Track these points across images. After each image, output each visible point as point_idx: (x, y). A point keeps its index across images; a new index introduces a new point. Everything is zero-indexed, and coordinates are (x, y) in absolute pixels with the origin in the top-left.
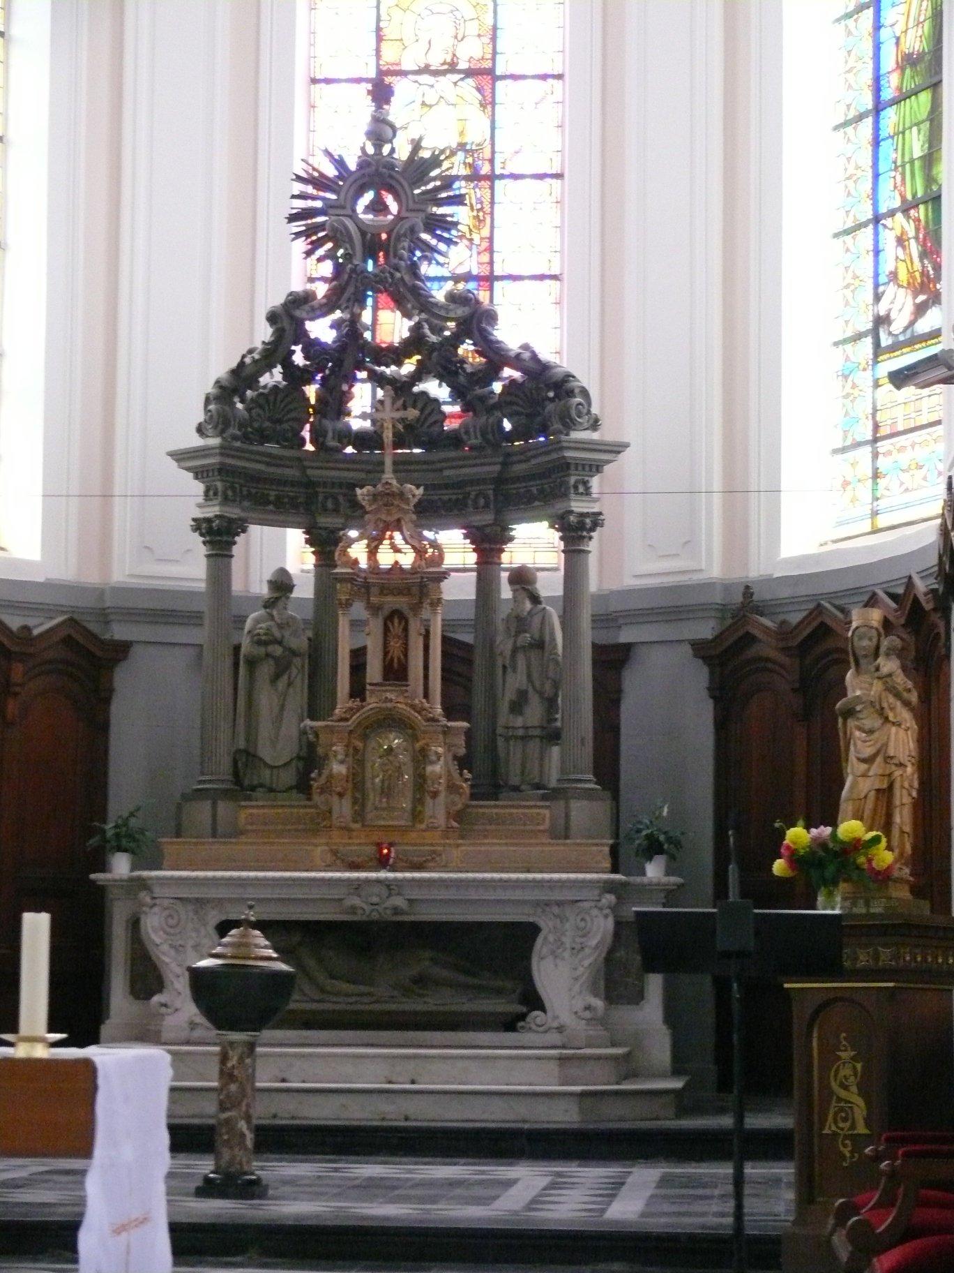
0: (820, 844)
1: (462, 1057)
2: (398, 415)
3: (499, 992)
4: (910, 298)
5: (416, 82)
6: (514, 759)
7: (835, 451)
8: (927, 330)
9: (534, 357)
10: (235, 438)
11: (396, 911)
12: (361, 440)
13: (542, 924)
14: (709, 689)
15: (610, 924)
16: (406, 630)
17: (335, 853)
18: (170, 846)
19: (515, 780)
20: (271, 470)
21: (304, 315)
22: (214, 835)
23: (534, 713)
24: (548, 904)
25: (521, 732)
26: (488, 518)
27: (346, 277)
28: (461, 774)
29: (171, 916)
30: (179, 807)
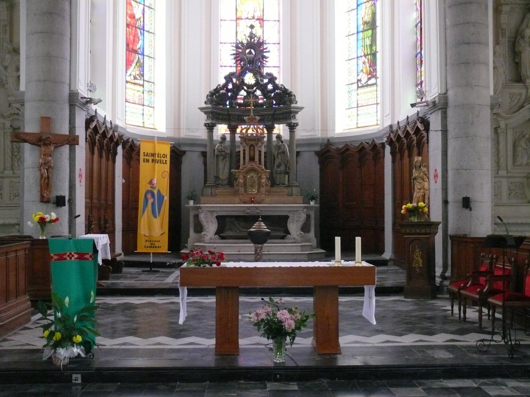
1: (279, 246)
2: (254, 100)
3: (279, 231)
4: (366, 76)
6: (278, 178)
7: (346, 109)
8: (371, 83)
9: (284, 88)
10: (214, 105)
11: (258, 213)
12: (240, 105)
13: (289, 215)
14: (319, 162)
15: (305, 216)
16: (254, 149)
17: (240, 200)
18: (202, 199)
19: (278, 183)
20: (222, 112)
22: (212, 196)
23: (282, 168)
24: (291, 211)
26: (270, 123)
27: (244, 69)
30: (202, 190)
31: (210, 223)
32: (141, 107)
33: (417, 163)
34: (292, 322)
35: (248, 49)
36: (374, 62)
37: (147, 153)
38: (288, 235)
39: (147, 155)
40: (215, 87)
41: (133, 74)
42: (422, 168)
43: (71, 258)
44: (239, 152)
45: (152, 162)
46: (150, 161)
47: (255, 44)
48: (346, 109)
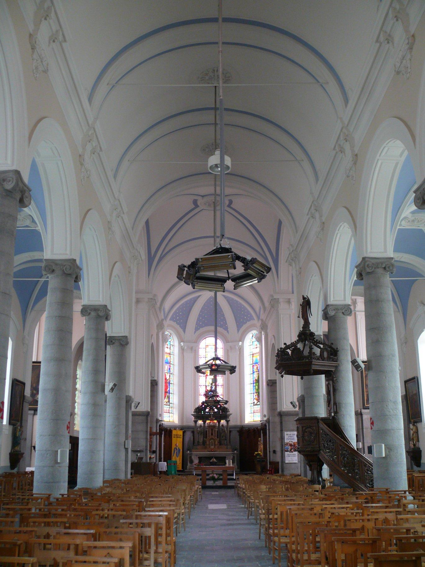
12: (207, 412)
32: (169, 414)
40: (197, 406)
44: (207, 431)
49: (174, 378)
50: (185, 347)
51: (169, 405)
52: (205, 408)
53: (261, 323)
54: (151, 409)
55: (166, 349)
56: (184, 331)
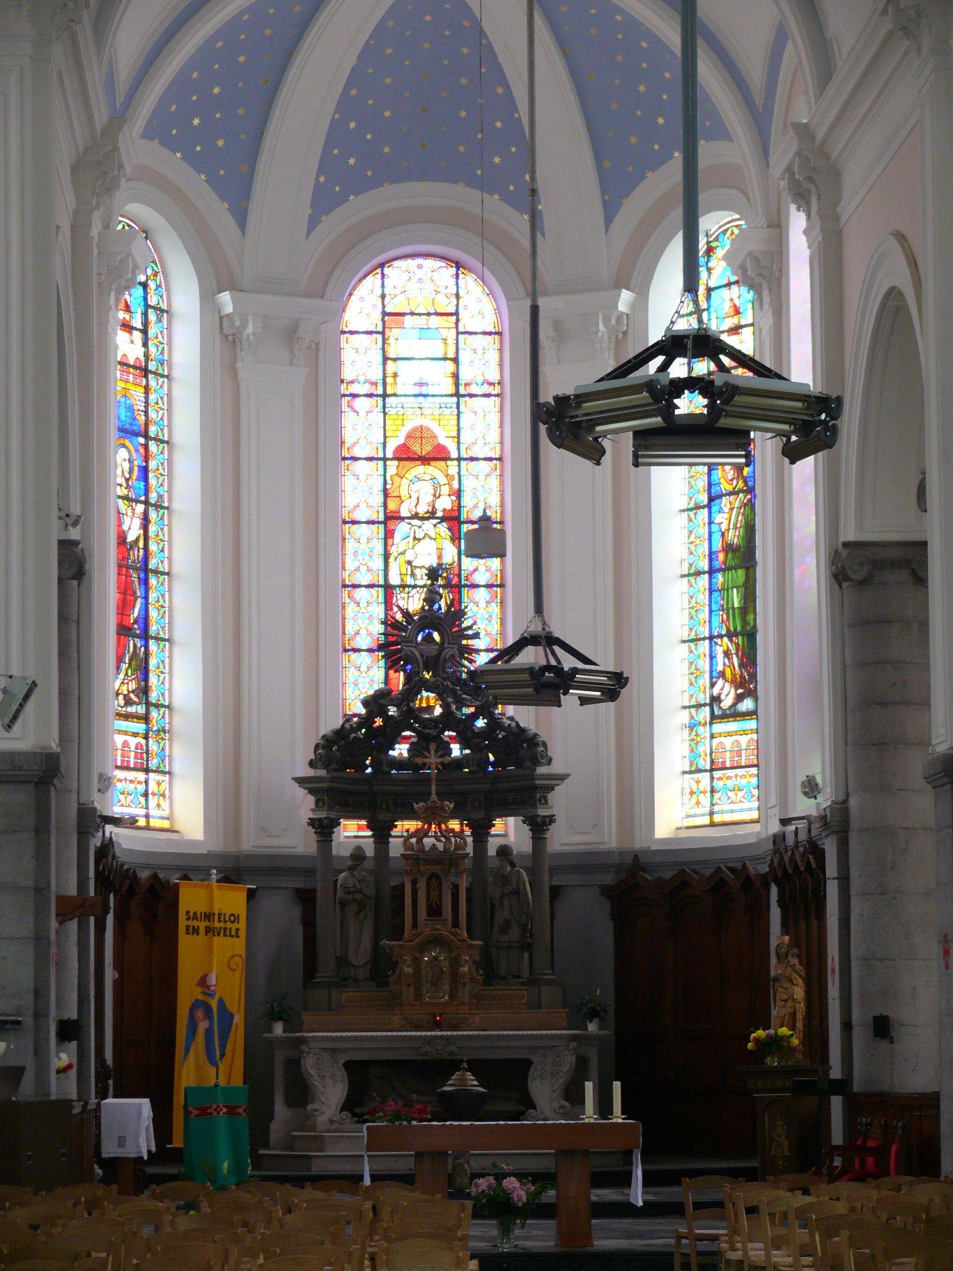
0: (768, 1036)
2: (439, 760)
4: (733, 691)
5: (410, 524)
7: (684, 773)
11: (451, 1053)
13: (532, 1059)
16: (440, 885)
18: (307, 1018)
19: (503, 973)
21: (386, 703)
23: (515, 934)
25: (506, 945)
26: (481, 815)
28: (477, 971)
29: (319, 1059)
31: (329, 1082)
32: (141, 776)
33: (781, 948)
34: (523, 1193)
35: (423, 630)
36: (752, 656)
37: (195, 913)
38: (531, 1110)
39: (195, 917)
41: (124, 690)
42: (789, 958)
43: (218, 1113)
44: (402, 886)
45: (206, 933)
46: (202, 930)
47: (440, 619)
48: (684, 773)
49: (175, 533)
50: (244, 325)
51: (146, 719)
52: (390, 735)
53: (799, 153)
54: (63, 740)
55: (122, 337)
56: (241, 219)
